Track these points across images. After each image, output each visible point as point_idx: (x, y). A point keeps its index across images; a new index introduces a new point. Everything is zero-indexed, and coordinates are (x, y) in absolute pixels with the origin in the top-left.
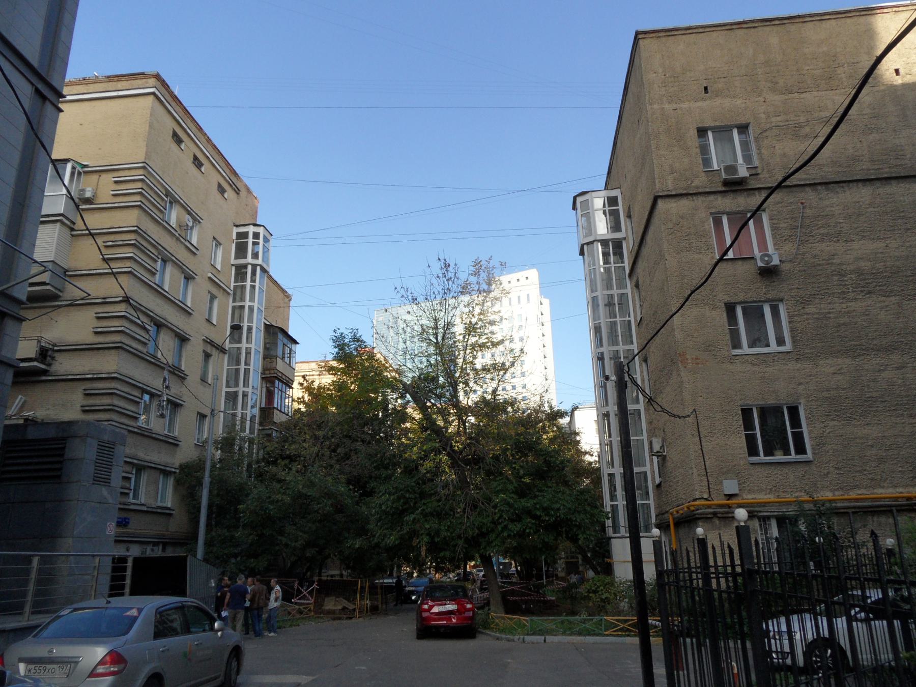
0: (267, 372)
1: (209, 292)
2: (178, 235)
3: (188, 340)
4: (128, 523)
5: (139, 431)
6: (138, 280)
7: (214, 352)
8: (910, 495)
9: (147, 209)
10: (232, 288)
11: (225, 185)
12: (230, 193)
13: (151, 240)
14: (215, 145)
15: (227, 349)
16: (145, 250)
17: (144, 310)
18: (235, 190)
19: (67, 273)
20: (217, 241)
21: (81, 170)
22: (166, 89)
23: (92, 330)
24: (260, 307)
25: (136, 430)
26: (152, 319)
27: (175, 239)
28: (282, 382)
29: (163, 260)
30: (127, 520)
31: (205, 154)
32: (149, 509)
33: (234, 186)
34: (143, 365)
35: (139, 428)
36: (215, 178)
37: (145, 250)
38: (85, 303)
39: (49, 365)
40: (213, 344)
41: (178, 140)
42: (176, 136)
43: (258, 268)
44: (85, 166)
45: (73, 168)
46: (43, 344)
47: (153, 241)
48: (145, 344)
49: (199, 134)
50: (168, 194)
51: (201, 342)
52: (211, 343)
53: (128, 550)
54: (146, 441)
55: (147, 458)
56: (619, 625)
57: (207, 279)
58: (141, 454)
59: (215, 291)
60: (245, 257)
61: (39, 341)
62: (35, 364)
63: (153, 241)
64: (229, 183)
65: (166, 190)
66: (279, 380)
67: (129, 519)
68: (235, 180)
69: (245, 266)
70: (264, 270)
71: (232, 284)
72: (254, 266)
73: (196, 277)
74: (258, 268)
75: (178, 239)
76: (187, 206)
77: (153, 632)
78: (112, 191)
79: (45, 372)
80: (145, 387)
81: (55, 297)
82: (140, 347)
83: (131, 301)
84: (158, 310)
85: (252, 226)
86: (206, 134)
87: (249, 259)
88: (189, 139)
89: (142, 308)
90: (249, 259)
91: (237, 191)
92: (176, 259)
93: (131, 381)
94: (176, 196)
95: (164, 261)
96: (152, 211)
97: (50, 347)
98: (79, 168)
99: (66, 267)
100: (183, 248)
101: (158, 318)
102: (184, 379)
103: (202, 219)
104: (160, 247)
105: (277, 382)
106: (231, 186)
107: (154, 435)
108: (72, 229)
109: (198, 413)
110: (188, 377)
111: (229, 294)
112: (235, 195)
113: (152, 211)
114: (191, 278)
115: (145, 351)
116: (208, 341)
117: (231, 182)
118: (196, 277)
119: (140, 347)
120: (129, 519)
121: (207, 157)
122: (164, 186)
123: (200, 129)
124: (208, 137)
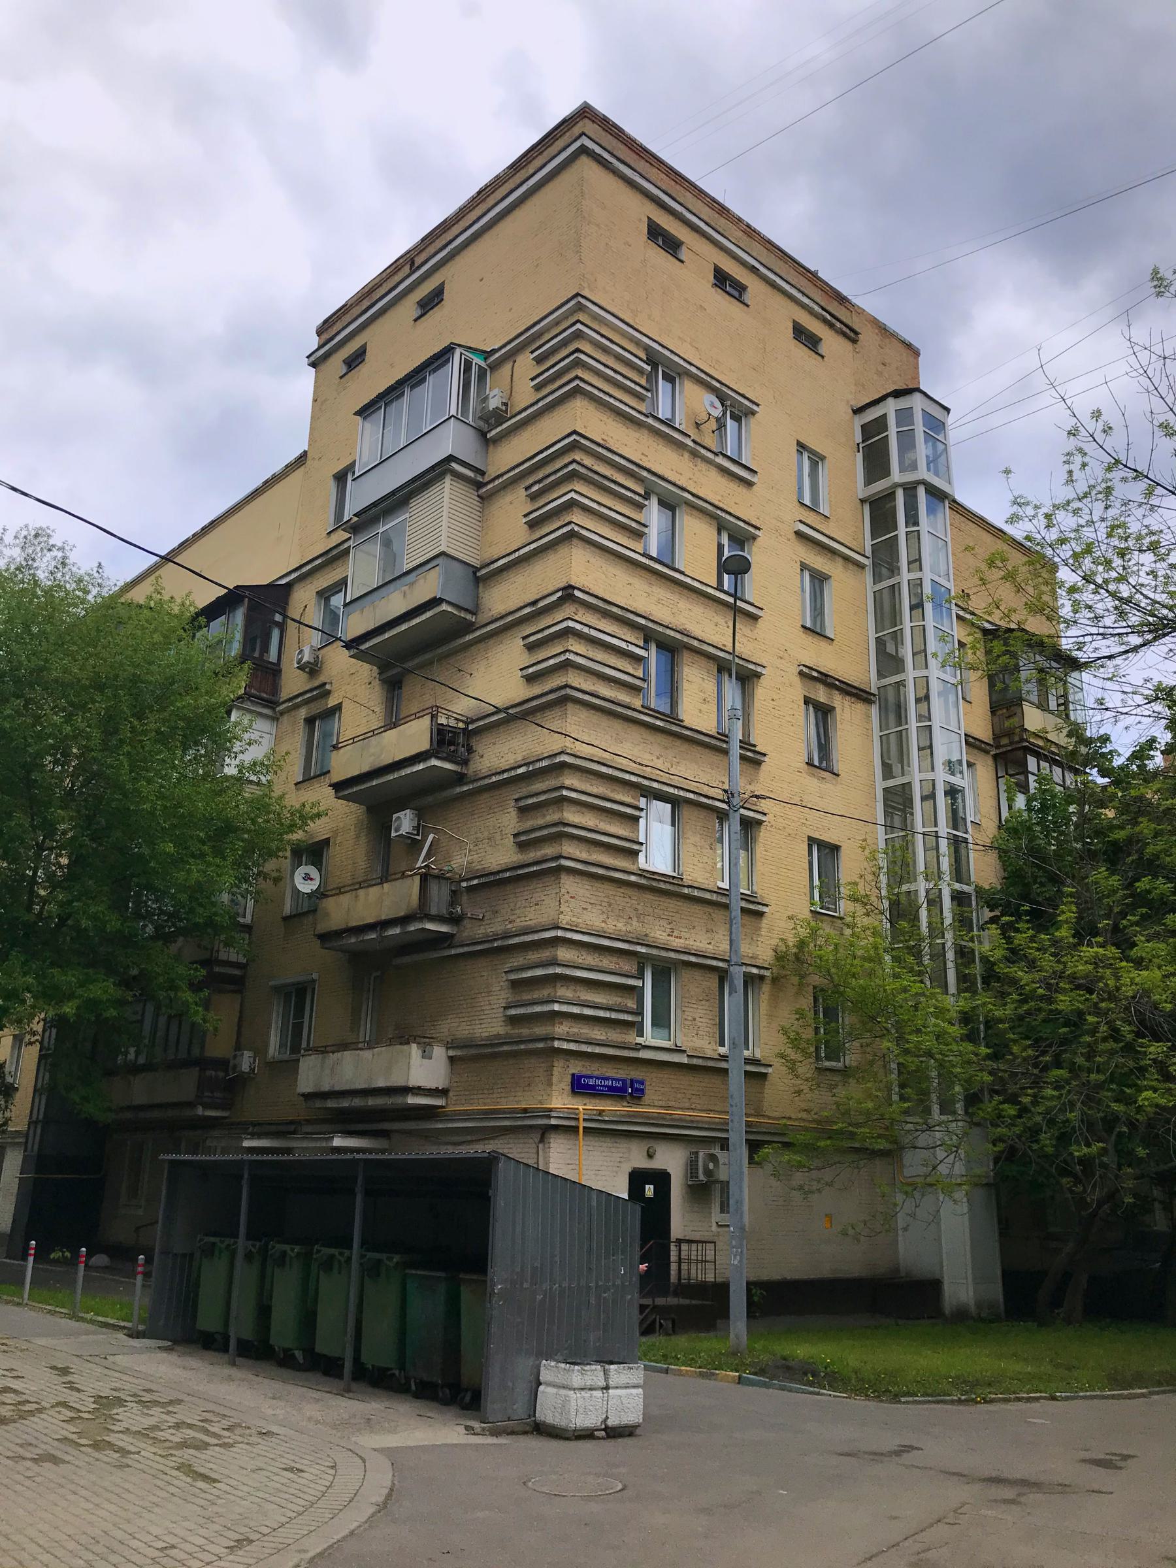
0: (1005, 741)
1: (804, 567)
2: (691, 444)
3: (758, 675)
4: (642, 1091)
5: (644, 881)
6: (612, 558)
7: (838, 701)
8: (659, 1075)
9: (596, 392)
10: (868, 552)
11: (815, 327)
12: (831, 342)
13: (617, 459)
14: (769, 242)
15: (874, 690)
16: (606, 483)
17: (620, 612)
18: (844, 335)
19: (478, 574)
20: (812, 452)
21: (483, 364)
22: (617, 137)
23: (520, 673)
24: (936, 578)
25: (633, 878)
26: (649, 637)
27: (686, 455)
28: (1046, 759)
29: (662, 503)
30: (637, 1086)
31: (744, 263)
32: (695, 1061)
33: (838, 325)
34: (636, 733)
35: (643, 873)
36: (783, 314)
37: (606, 483)
38: (508, 625)
39: (465, 762)
40: (830, 680)
41: (671, 246)
42: (655, 233)
43: (921, 492)
44: (494, 351)
45: (468, 365)
46: (442, 720)
47: (623, 462)
48: (636, 689)
49: (722, 223)
50: (653, 360)
51: (796, 680)
52: (824, 679)
53: (650, 1156)
54: (672, 904)
55: (676, 943)
56: (957, 615)
57: (793, 536)
58: (659, 934)
59: (819, 562)
60: (887, 473)
61: (434, 717)
62: (434, 762)
63: (623, 462)
64: (825, 321)
65: (647, 349)
66: (1038, 756)
67: (642, 1083)
68: (841, 313)
69: (890, 496)
70: (937, 495)
71: (868, 543)
72: (910, 489)
73: (757, 532)
74: (921, 492)
75: (694, 454)
76: (709, 379)
77: (999, 1272)
78: (532, 379)
79: (460, 778)
80: (646, 782)
81: (469, 627)
82: (623, 696)
83: (577, 593)
84: (662, 614)
85: (890, 400)
86: (740, 220)
87: (896, 476)
88: (696, 236)
89: (615, 609)
90: (896, 476)
91: (851, 335)
92: (693, 495)
93: (604, 769)
94: (676, 359)
95: (669, 505)
96: (611, 396)
97: (461, 725)
98: (477, 360)
99: (477, 564)
100: (714, 474)
101: (660, 629)
102: (758, 763)
103: (758, 405)
104: (645, 474)
105: (1032, 762)
106: (831, 326)
107: (686, 891)
108: (479, 485)
109: (812, 841)
110: (766, 759)
111: (862, 567)
112: (848, 345)
113: (611, 396)
114: (748, 539)
115: (637, 703)
116: (815, 674)
117: (829, 317)
118: (757, 532)
119: (623, 696)
120: (642, 1083)
121: (754, 270)
122: (638, 343)
123: (723, 210)
124: (748, 226)
